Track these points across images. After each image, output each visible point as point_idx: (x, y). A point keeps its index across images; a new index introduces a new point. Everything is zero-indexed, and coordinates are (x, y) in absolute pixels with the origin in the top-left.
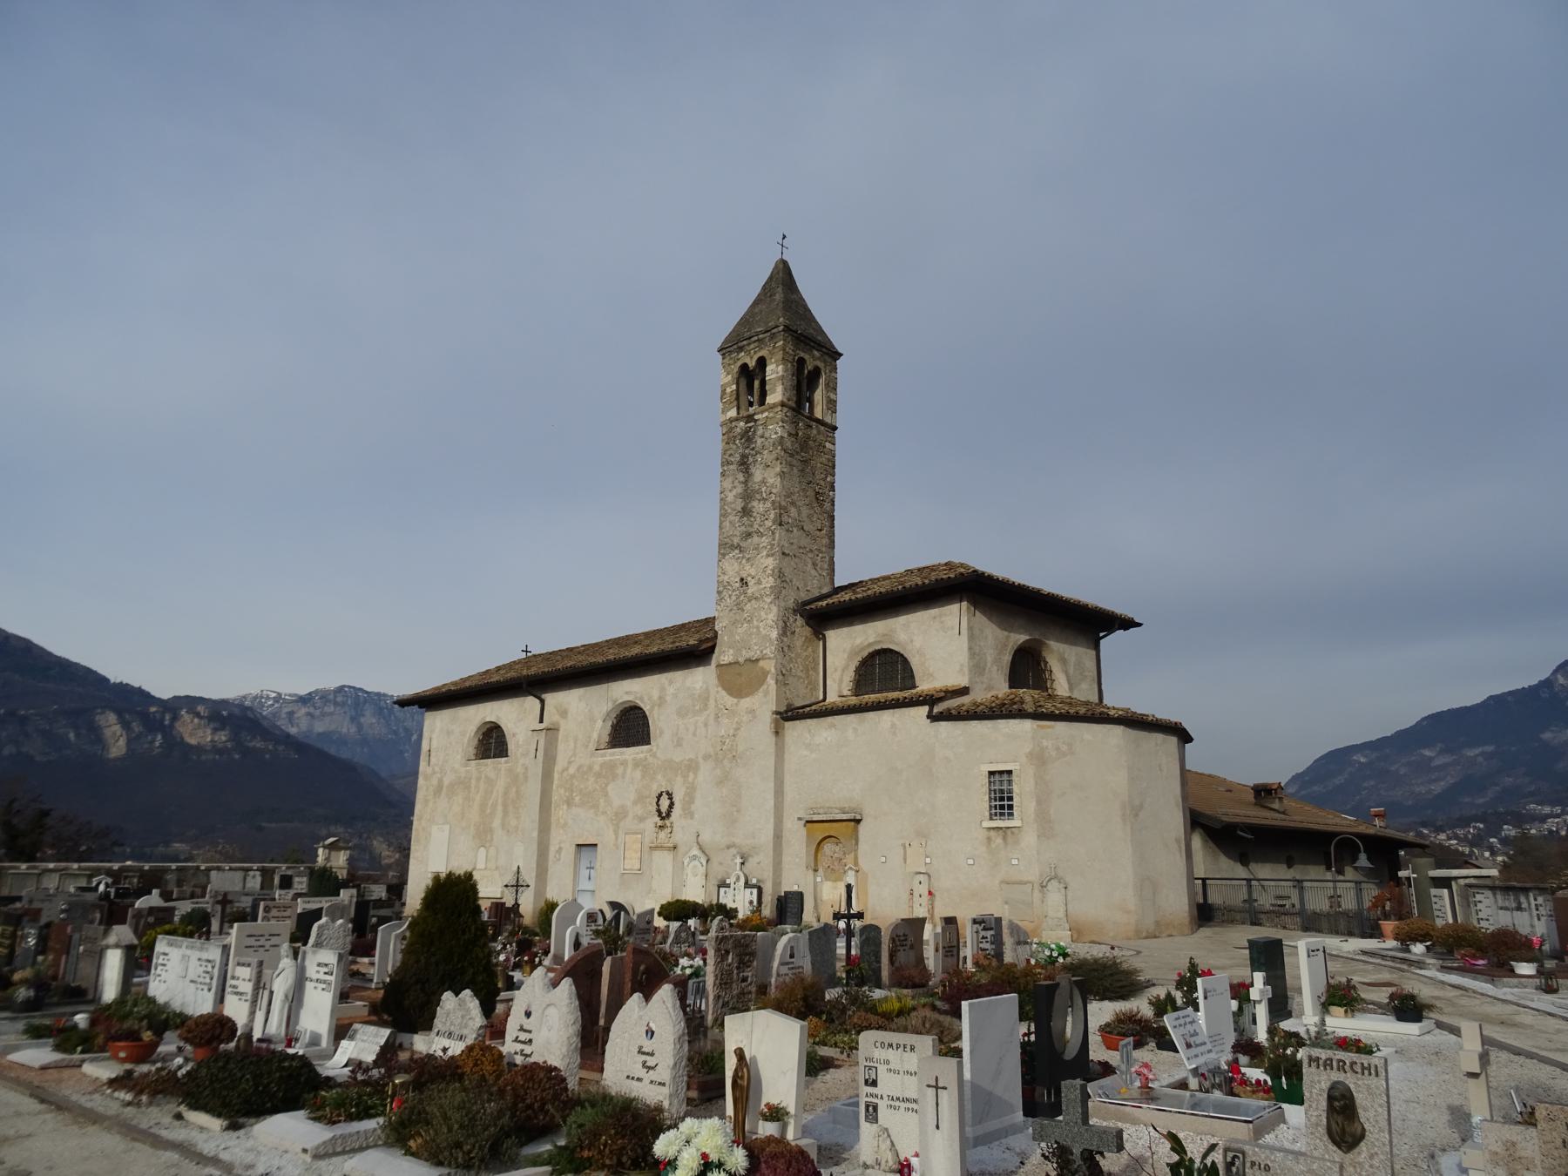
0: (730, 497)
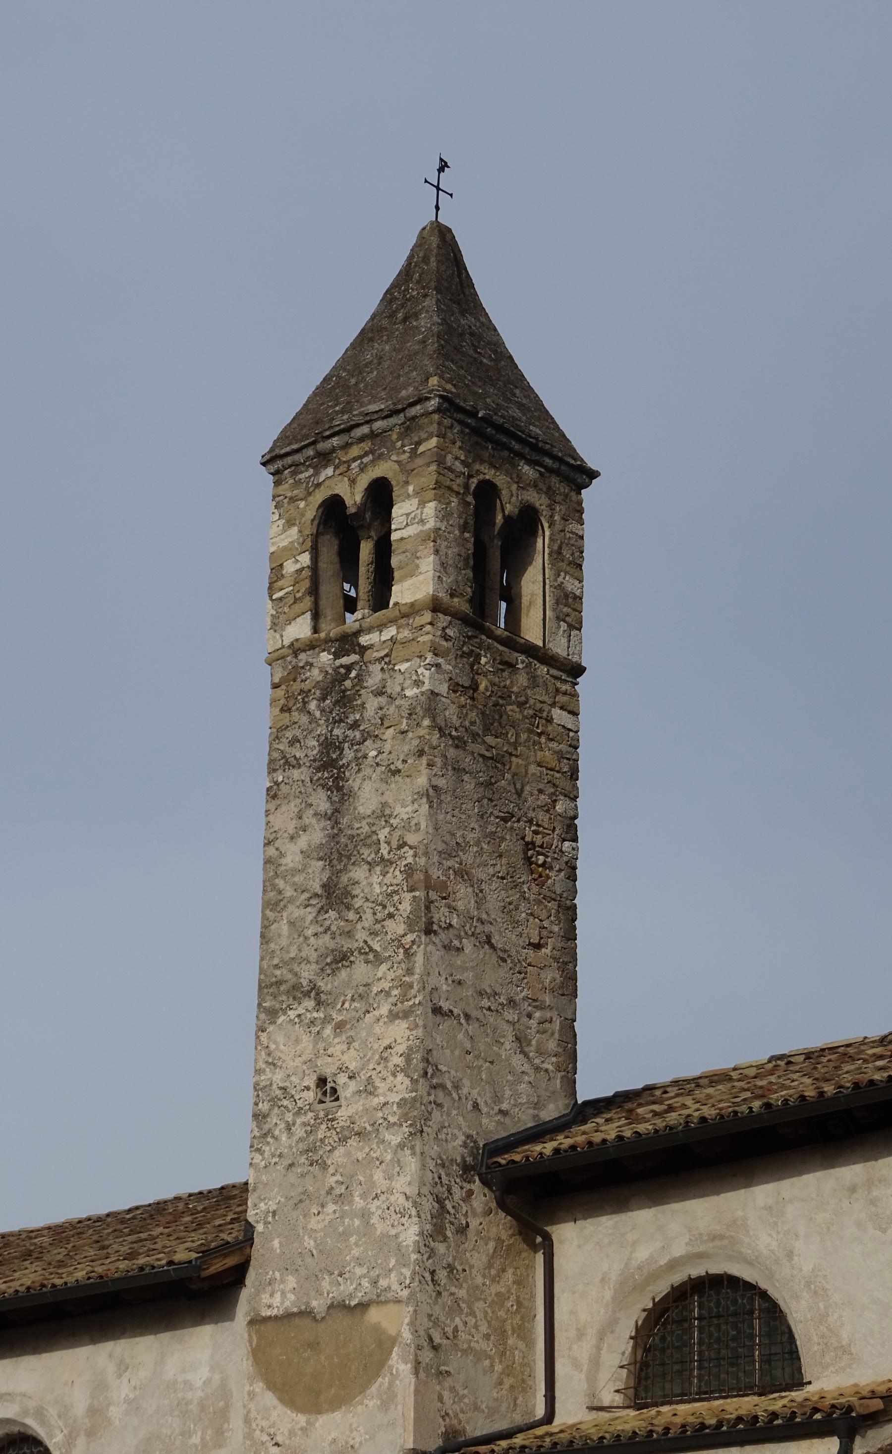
0: (292, 857)
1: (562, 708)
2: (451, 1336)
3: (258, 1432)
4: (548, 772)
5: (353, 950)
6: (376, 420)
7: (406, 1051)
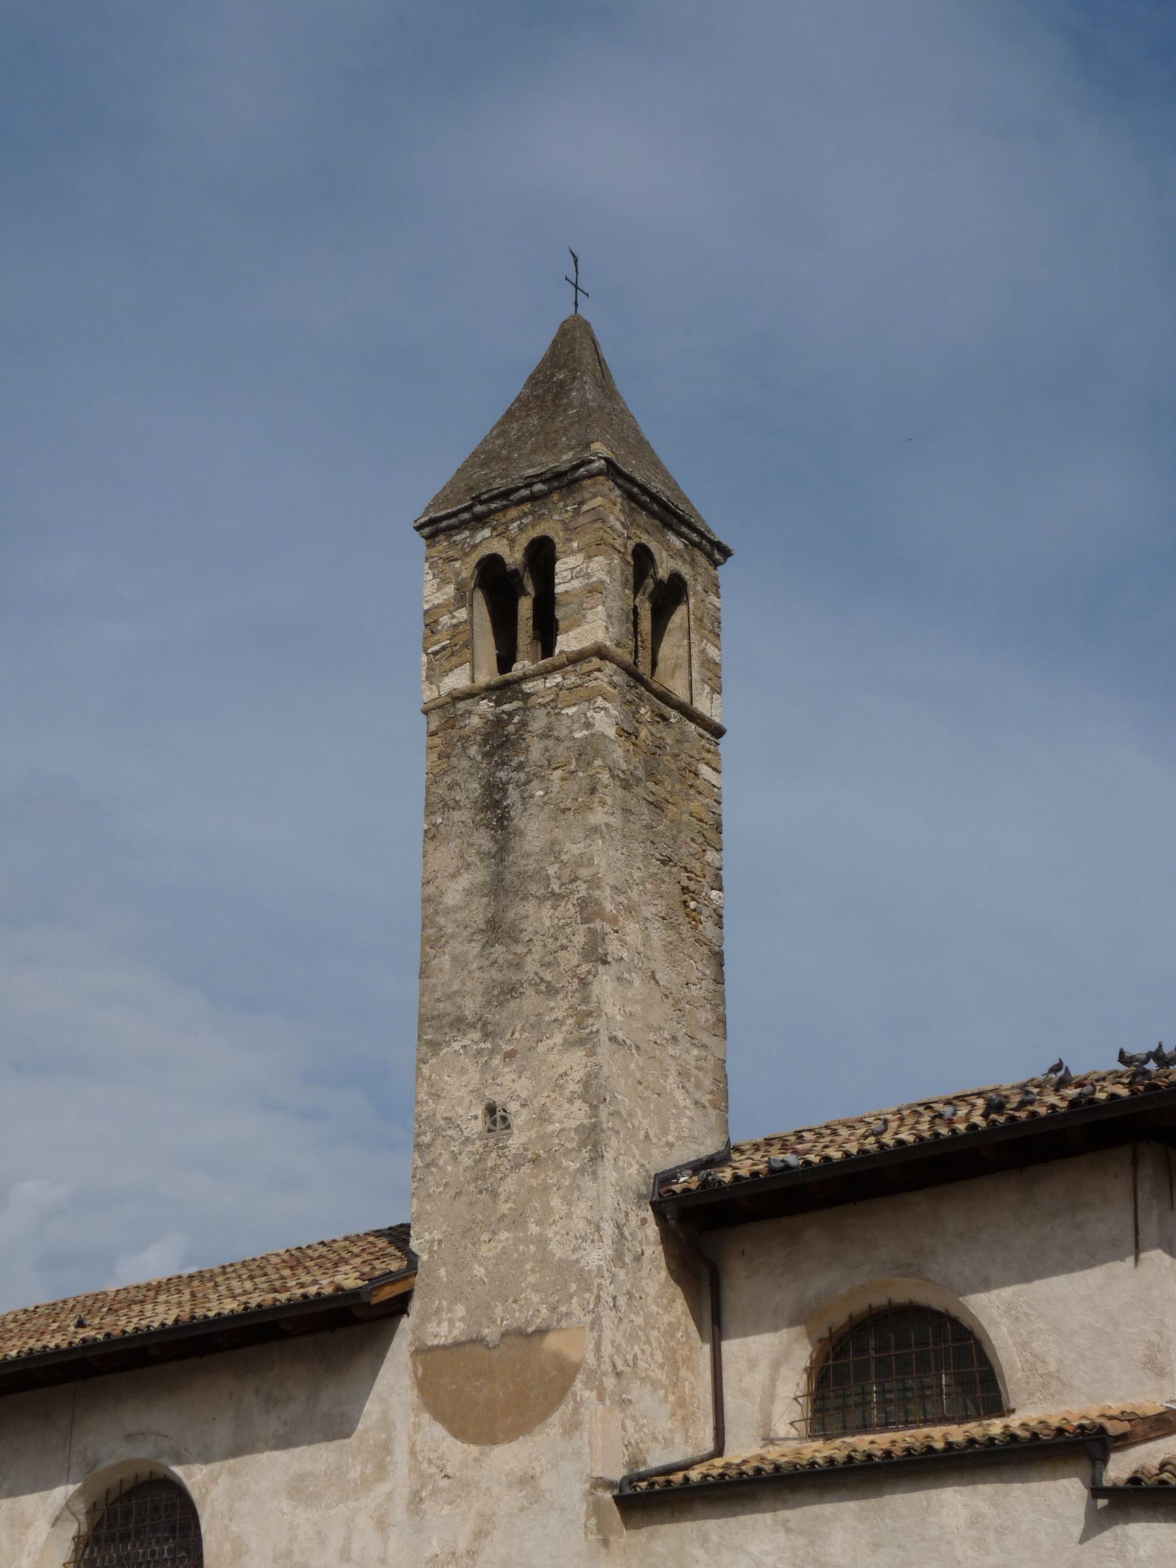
0: (453, 894)
1: (707, 764)
2: (632, 1365)
3: (425, 1465)
4: (698, 822)
5: (523, 981)
6: (535, 483)
7: (584, 1078)
